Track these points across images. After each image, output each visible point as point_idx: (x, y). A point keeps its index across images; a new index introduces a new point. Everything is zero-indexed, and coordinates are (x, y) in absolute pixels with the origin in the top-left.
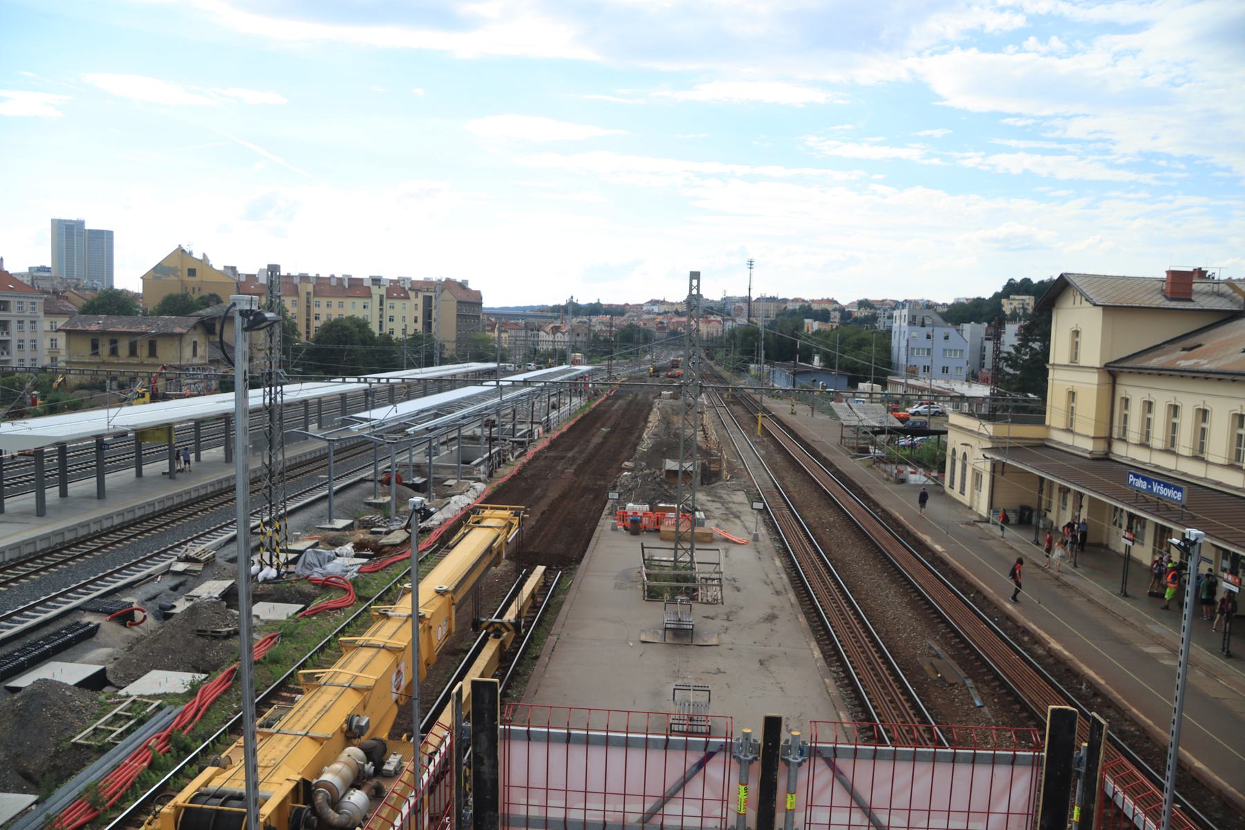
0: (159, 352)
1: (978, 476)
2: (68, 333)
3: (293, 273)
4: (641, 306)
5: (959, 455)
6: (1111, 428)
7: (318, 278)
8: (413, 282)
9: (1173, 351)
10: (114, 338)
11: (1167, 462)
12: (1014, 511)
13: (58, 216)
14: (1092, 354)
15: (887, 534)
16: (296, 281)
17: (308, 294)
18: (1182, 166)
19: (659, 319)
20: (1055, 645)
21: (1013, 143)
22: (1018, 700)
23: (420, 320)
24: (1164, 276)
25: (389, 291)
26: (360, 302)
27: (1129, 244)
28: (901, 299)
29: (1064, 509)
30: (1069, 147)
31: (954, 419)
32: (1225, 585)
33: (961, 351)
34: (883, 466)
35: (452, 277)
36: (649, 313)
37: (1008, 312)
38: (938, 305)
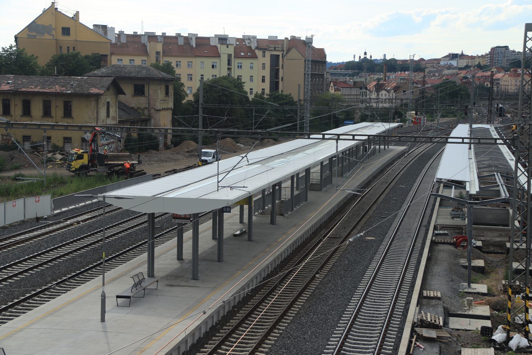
0: (75, 112)
4: (438, 60)
7: (164, 36)
8: (259, 41)
10: (47, 101)
16: (145, 40)
17: (158, 53)
19: (463, 74)
23: (268, 79)
25: (237, 50)
26: (209, 62)
33: (177, 62)
35: (297, 35)
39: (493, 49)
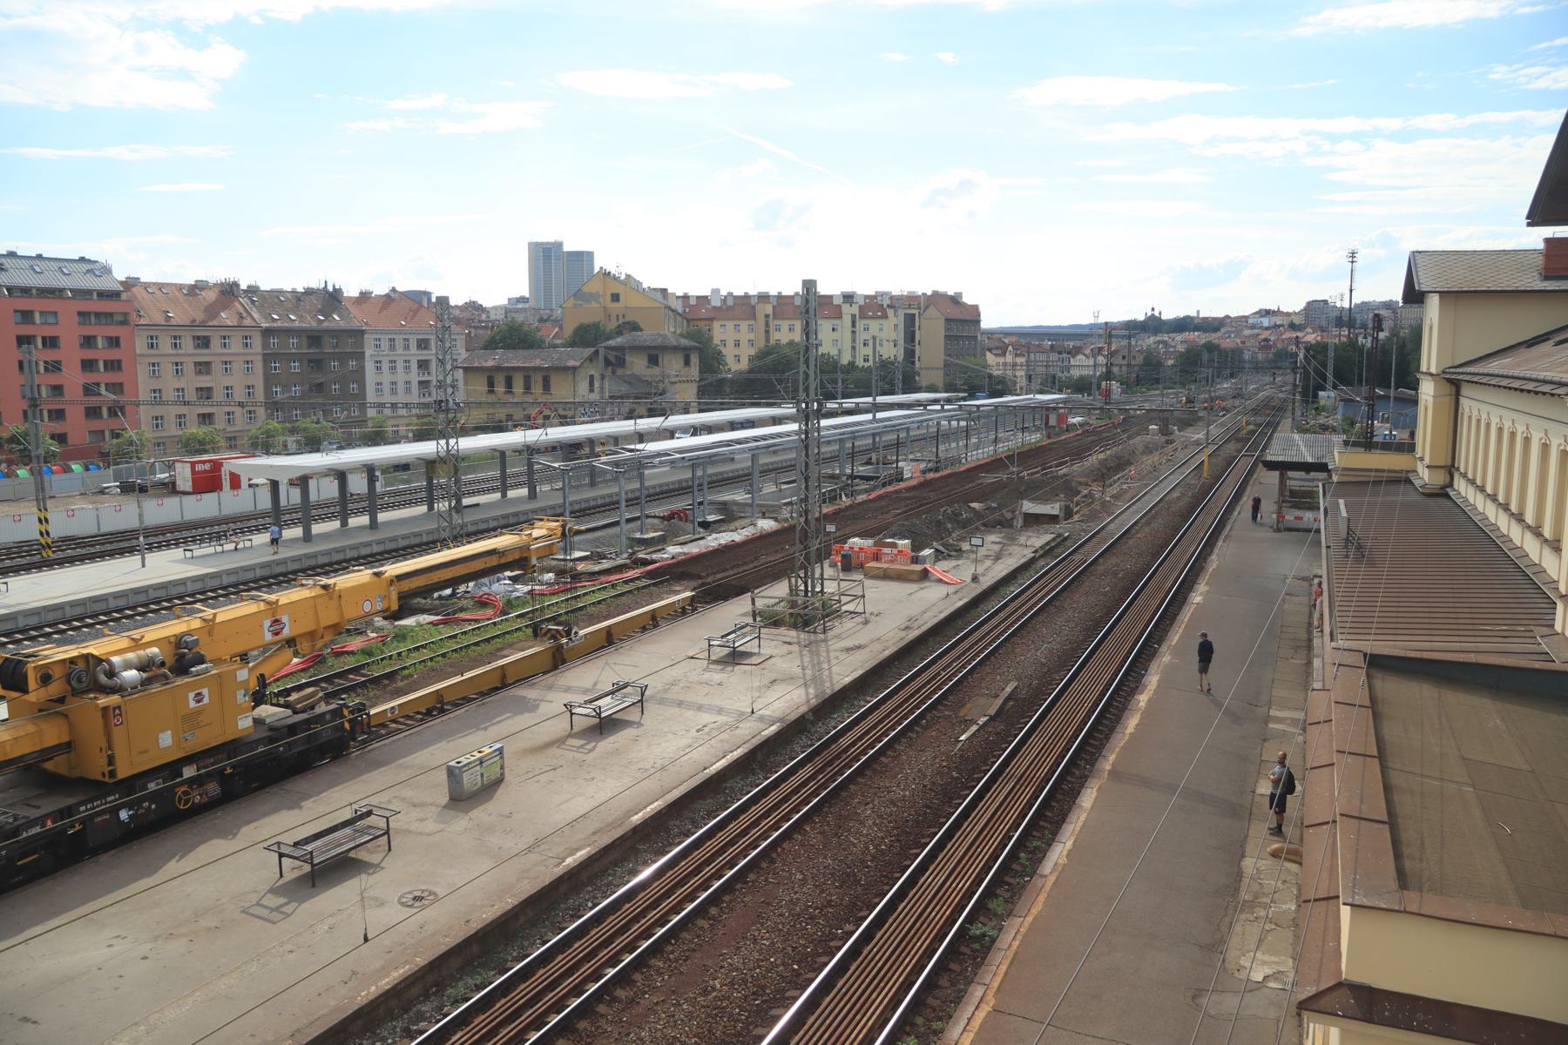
2: (466, 370)
3: (751, 293)
4: (1246, 318)
7: (780, 297)
8: (892, 298)
13: (535, 240)
16: (753, 302)
17: (767, 316)
19: (1266, 334)
24: (1541, 246)
35: (941, 289)
36: (1253, 327)
39: (1309, 303)
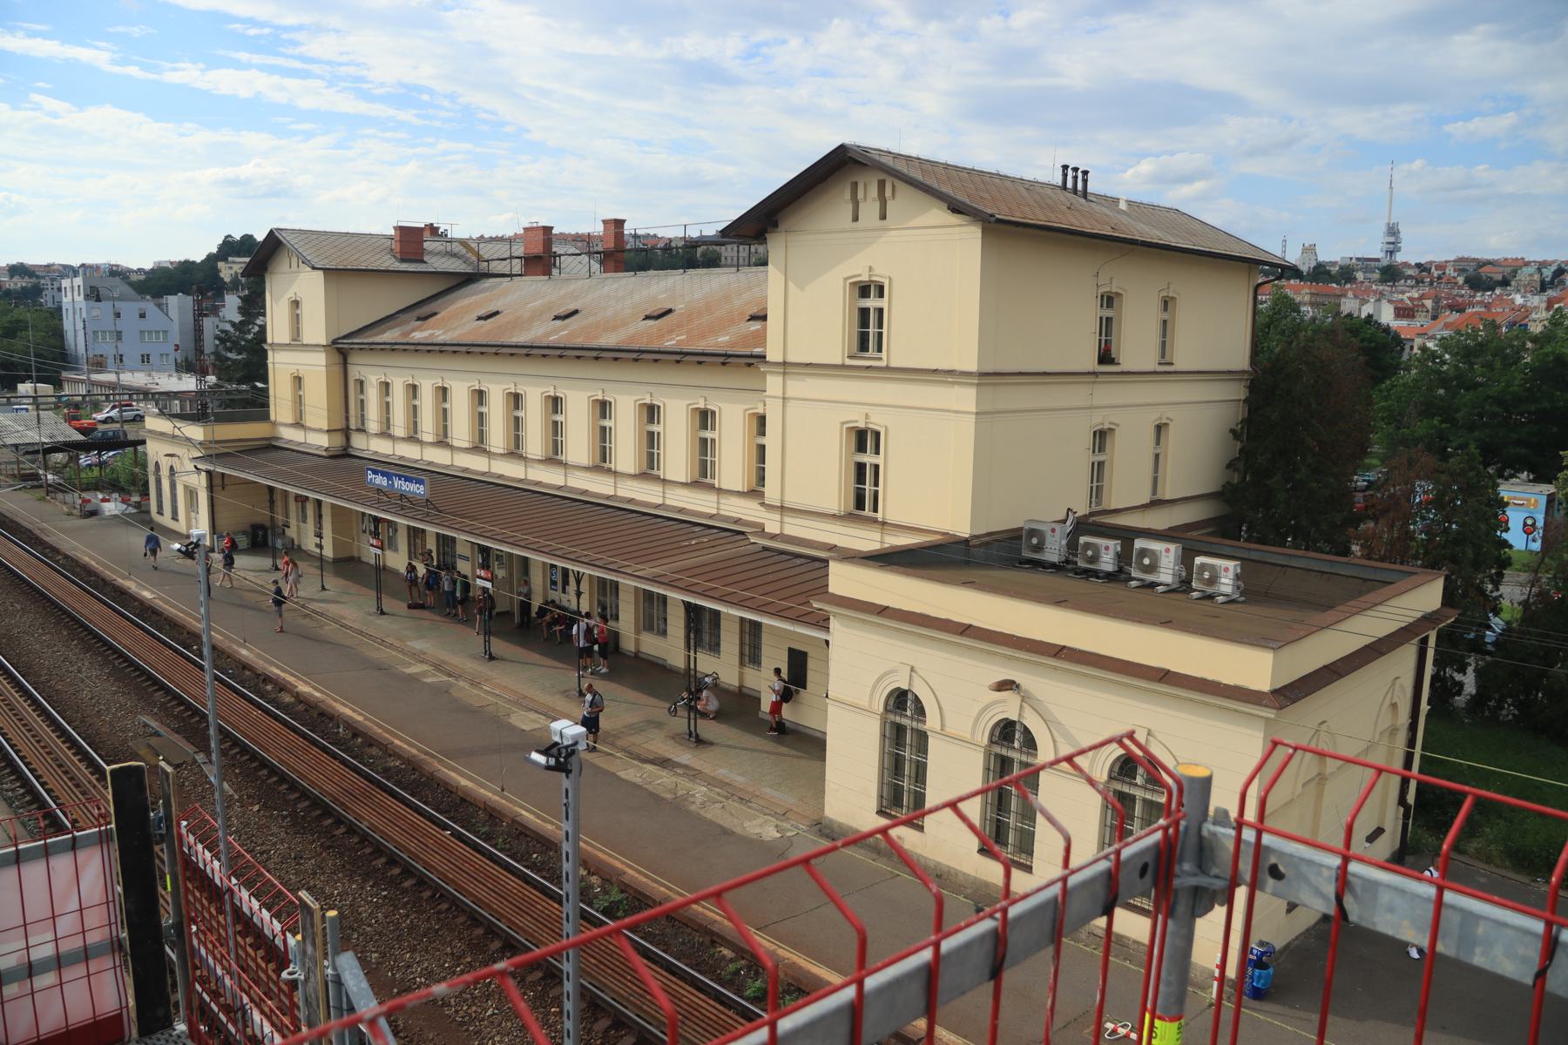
1: (191, 493)
5: (165, 472)
6: (347, 419)
9: (407, 322)
11: (409, 452)
12: (244, 533)
14: (316, 330)
15: (74, 588)
18: (446, 104)
20: (303, 688)
21: (244, 56)
22: (264, 764)
27: (360, 196)
28: (76, 263)
29: (304, 521)
30: (314, 68)
31: (154, 423)
32: (479, 582)
33: (165, 332)
34: (60, 496)
37: (227, 280)
38: (131, 271)
